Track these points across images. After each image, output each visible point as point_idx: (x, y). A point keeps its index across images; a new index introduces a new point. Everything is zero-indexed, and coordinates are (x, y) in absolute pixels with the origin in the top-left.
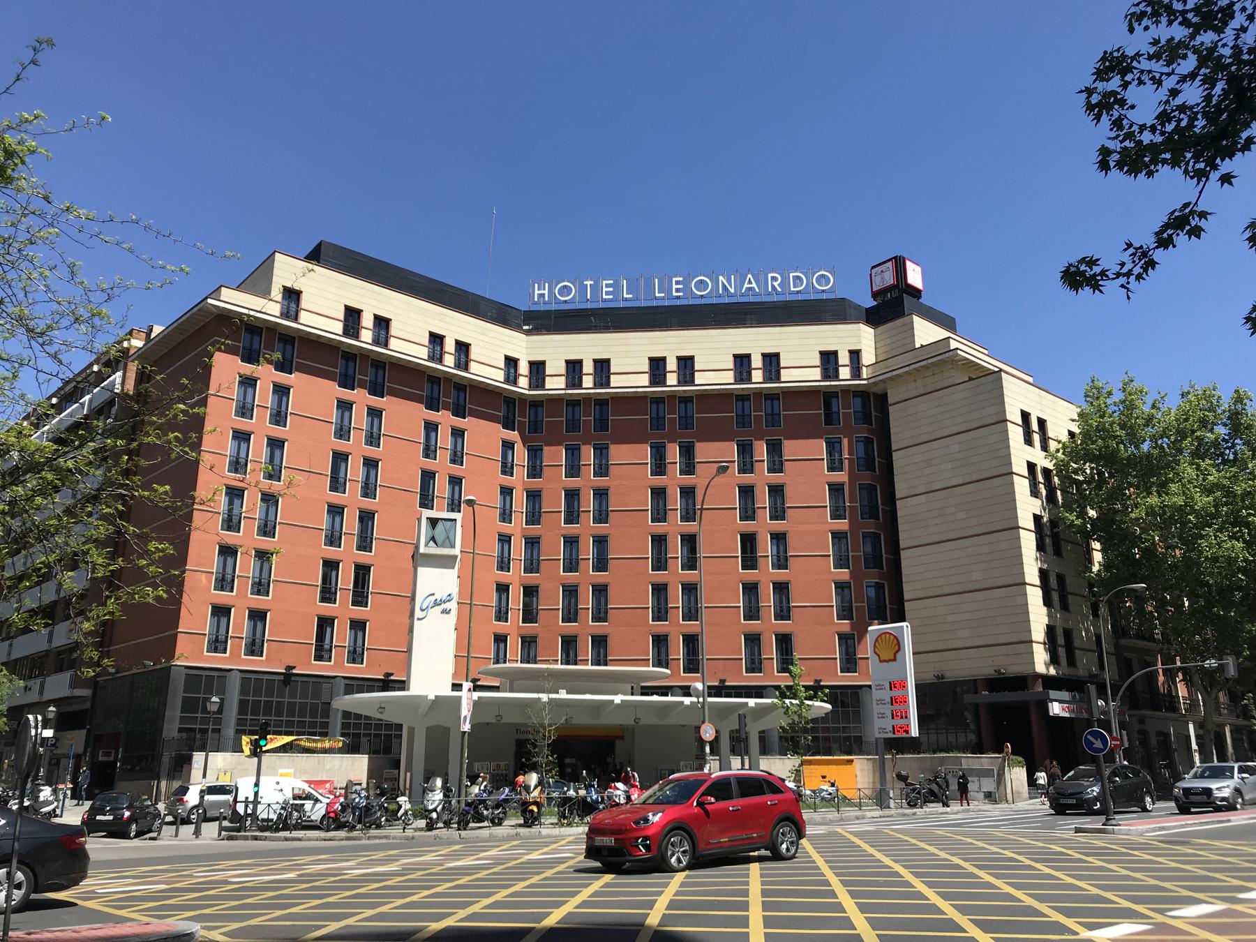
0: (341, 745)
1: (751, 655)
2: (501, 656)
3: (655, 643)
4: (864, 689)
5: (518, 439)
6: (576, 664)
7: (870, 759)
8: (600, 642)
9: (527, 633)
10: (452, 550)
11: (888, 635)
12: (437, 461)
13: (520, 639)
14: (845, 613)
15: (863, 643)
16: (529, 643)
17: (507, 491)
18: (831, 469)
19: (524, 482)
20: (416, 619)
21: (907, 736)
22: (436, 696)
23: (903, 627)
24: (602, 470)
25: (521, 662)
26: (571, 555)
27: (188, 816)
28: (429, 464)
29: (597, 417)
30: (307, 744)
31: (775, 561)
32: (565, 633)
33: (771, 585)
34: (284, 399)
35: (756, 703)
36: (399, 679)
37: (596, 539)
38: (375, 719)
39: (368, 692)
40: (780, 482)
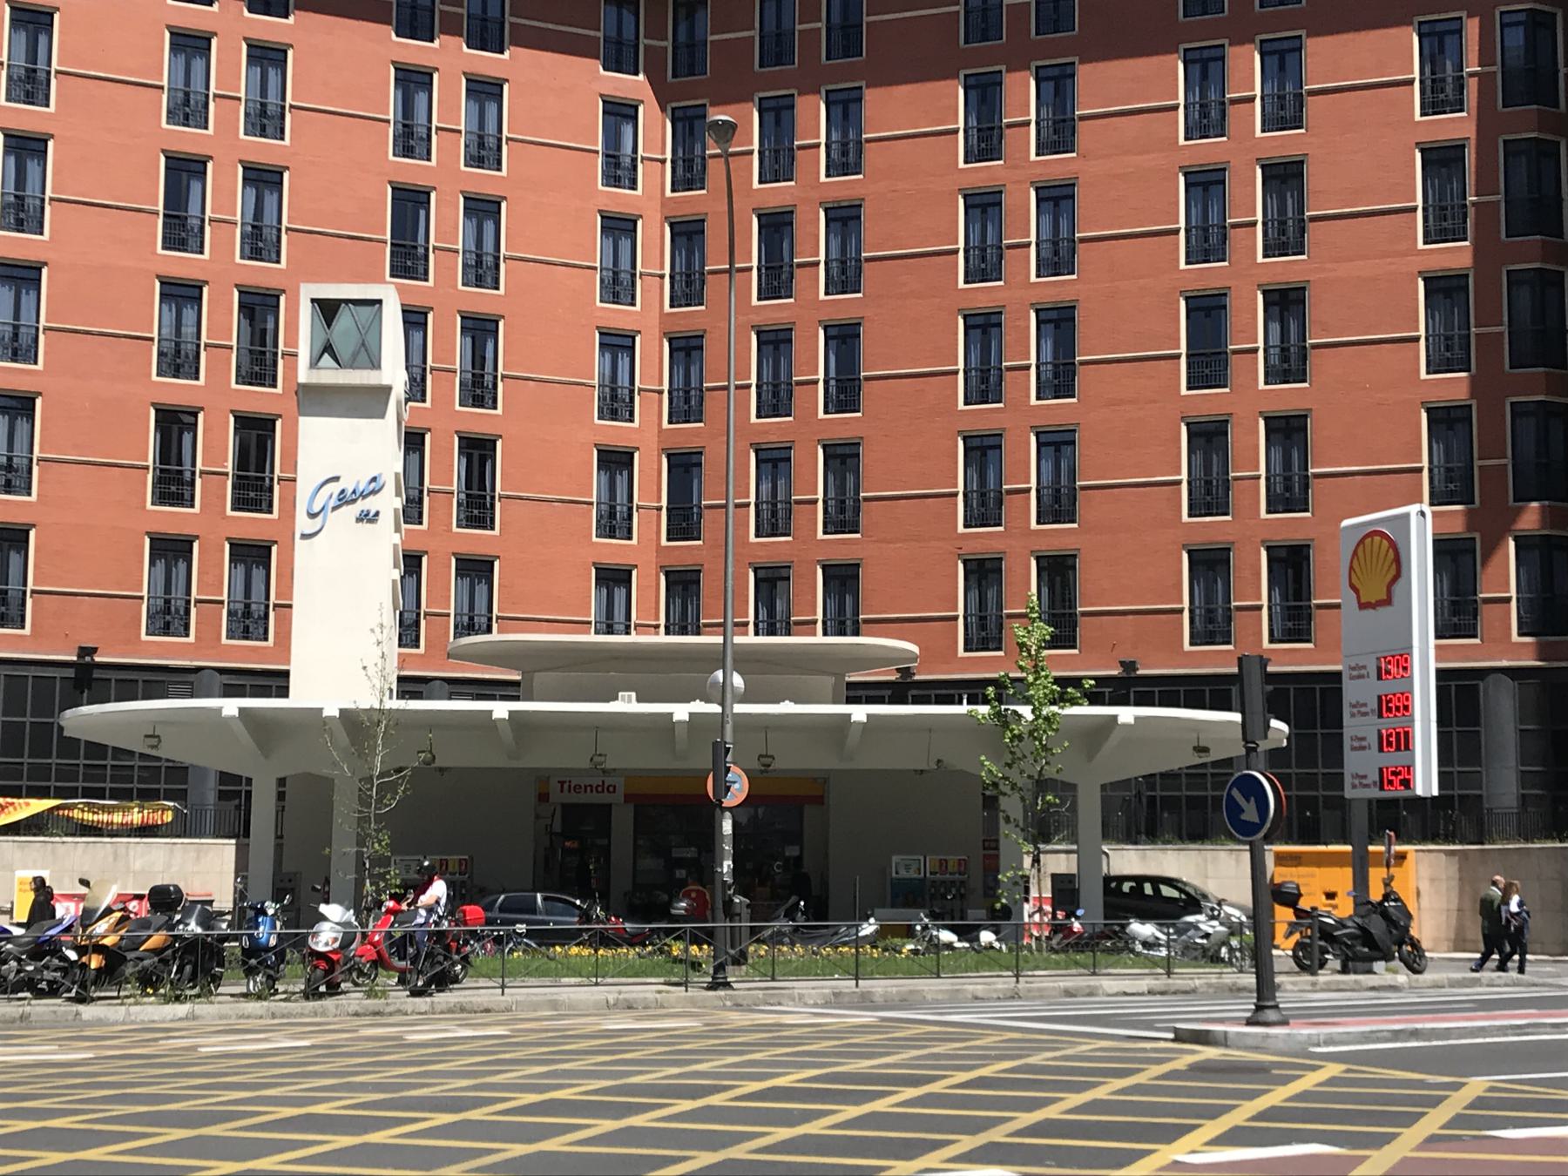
1: (1207, 603)
2: (619, 615)
4: (1491, 678)
5: (648, 94)
6: (698, 634)
7: (1452, 853)
8: (842, 579)
11: (1377, 539)
12: (434, 162)
13: (663, 578)
14: (1452, 486)
15: (1496, 560)
16: (683, 584)
17: (619, 227)
18: (1429, 107)
19: (665, 202)
20: (297, 536)
21: (1407, 793)
22: (341, 711)
23: (1407, 516)
24: (845, 160)
25: (667, 633)
28: (412, 170)
29: (836, 19)
30: (89, 817)
31: (1274, 360)
32: (764, 559)
33: (1262, 423)
34: (42, 39)
35: (1137, 718)
37: (833, 332)
40: (1293, 152)
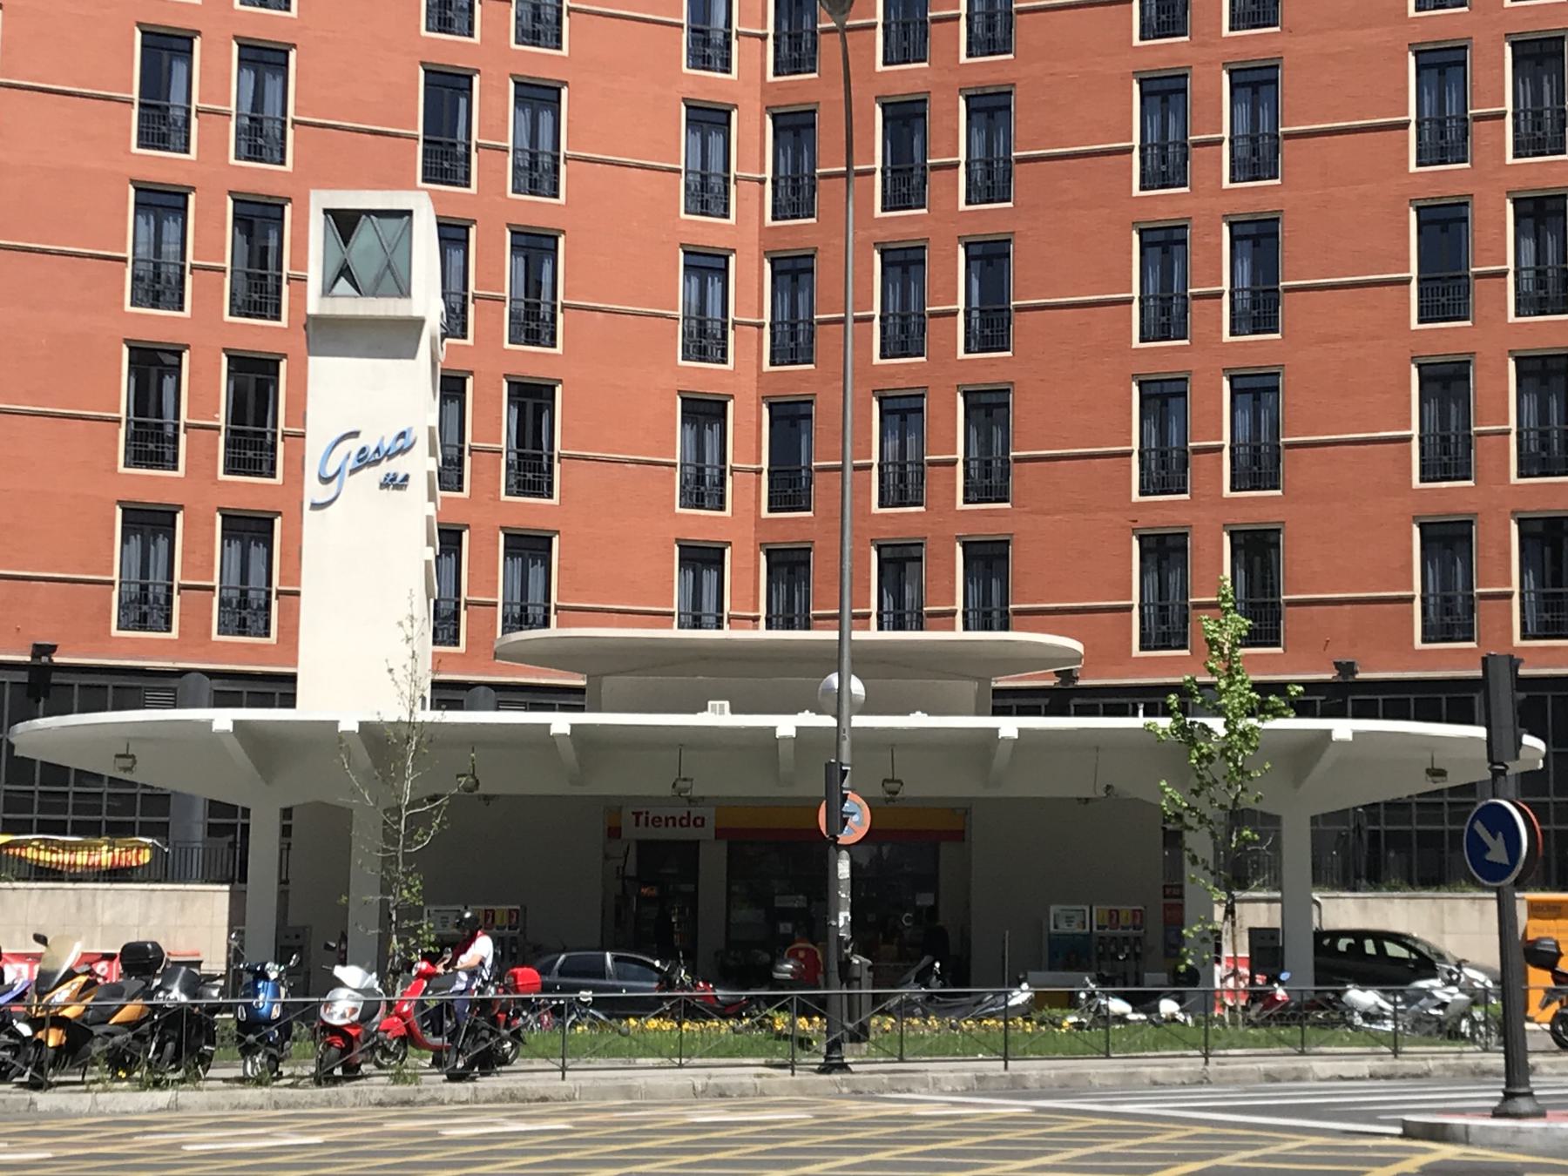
0: (145, 856)
2: (709, 605)
3: (1241, 554)
6: (808, 628)
9: (782, 539)
10: (402, 302)
12: (477, 39)
13: (763, 558)
19: (765, 87)
20: (307, 505)
22: (361, 724)
26: (905, 304)
27: (1094, 1023)
30: (45, 856)
33: (1512, 364)
35: (1020, 730)
36: (543, 681)
37: (976, 251)
38: (114, 781)
39: (84, 709)
